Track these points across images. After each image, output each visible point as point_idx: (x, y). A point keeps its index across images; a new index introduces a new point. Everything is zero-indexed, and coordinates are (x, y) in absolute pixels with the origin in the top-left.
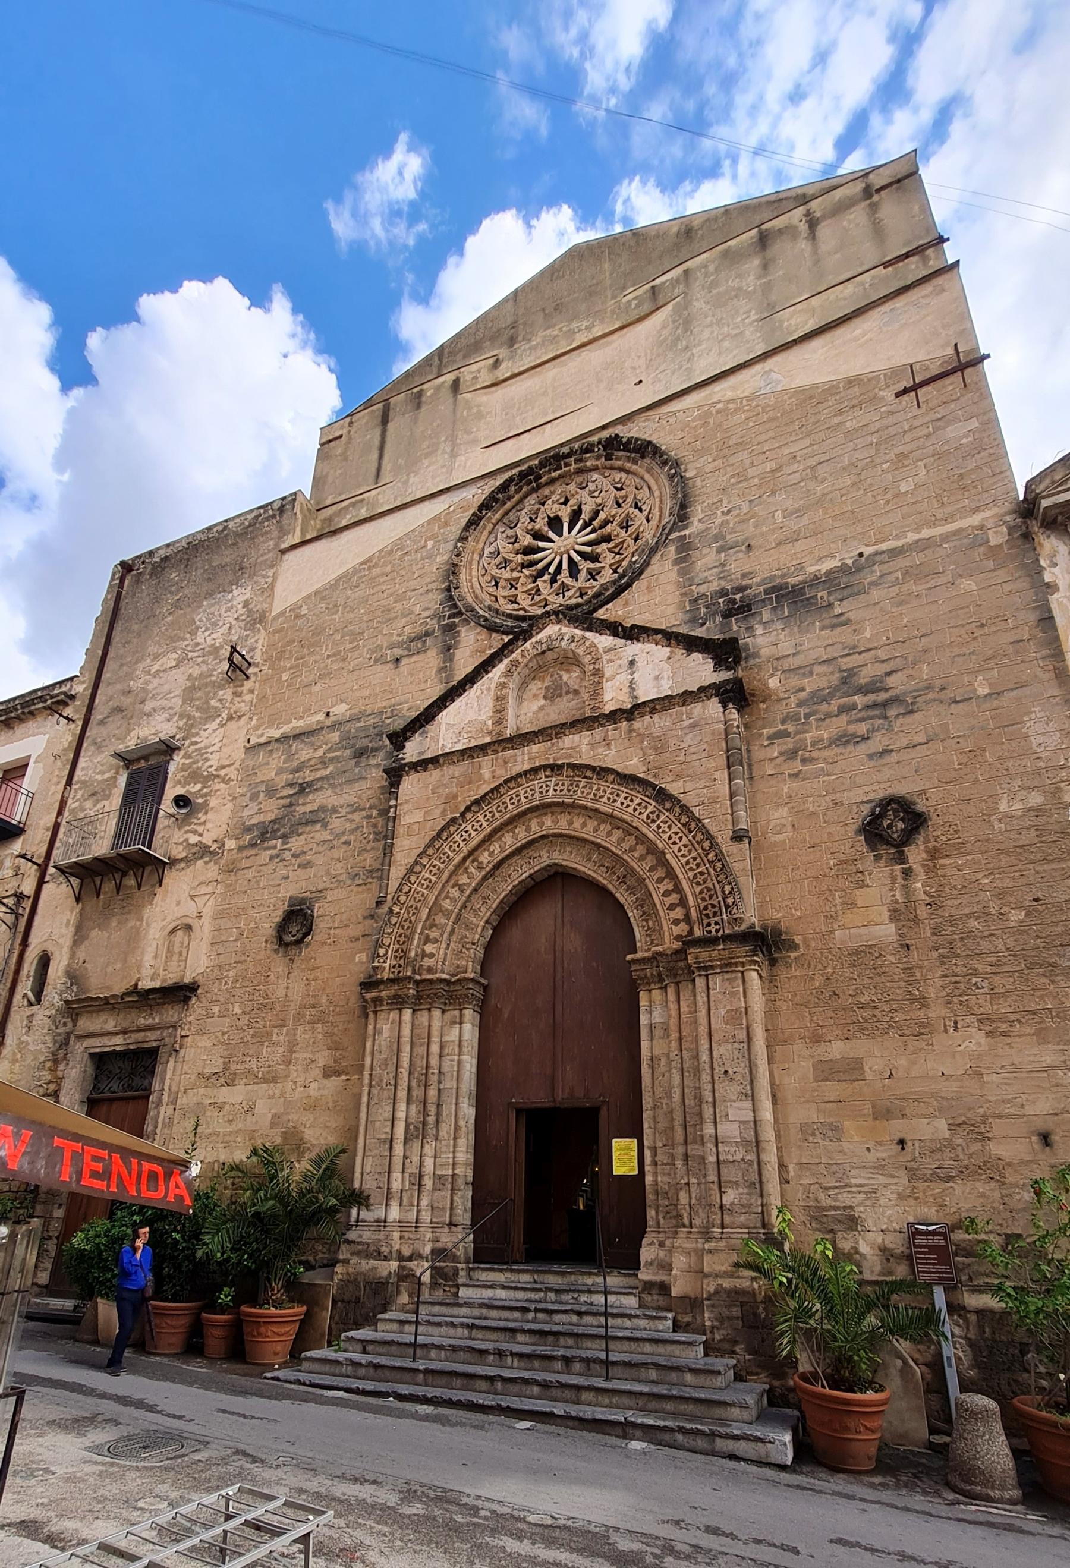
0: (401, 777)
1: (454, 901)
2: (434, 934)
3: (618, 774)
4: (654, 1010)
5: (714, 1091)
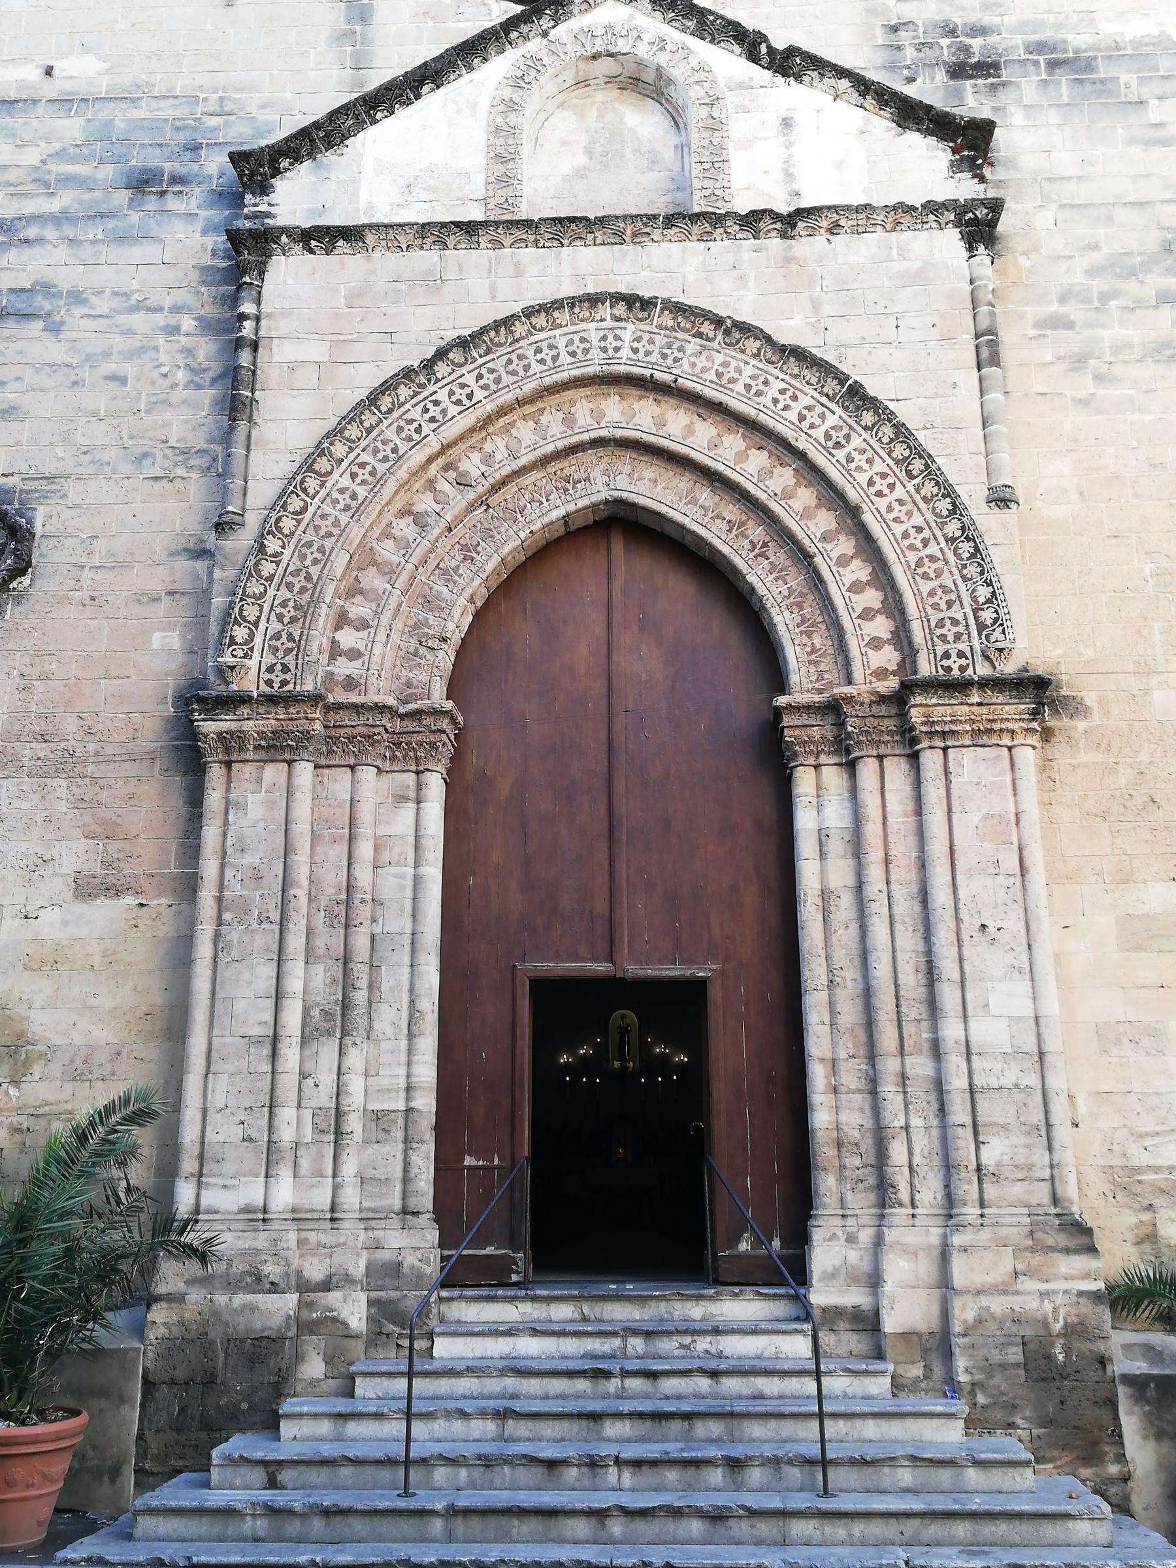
0: (268, 255)
1: (405, 546)
2: (359, 609)
3: (769, 339)
4: (819, 801)
5: (961, 961)
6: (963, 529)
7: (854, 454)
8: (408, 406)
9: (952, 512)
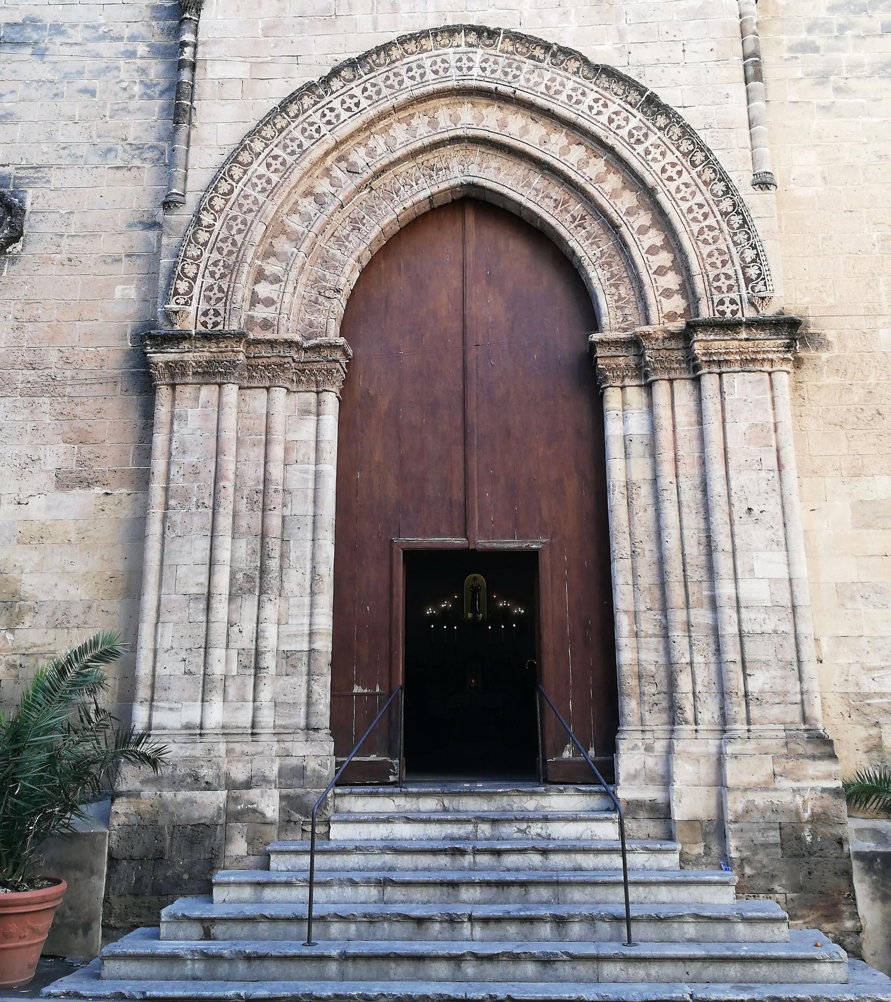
1: (308, 219)
2: (272, 267)
4: (624, 414)
5: (732, 535)
6: (734, 205)
7: (651, 148)
8: (310, 112)
9: (725, 193)
